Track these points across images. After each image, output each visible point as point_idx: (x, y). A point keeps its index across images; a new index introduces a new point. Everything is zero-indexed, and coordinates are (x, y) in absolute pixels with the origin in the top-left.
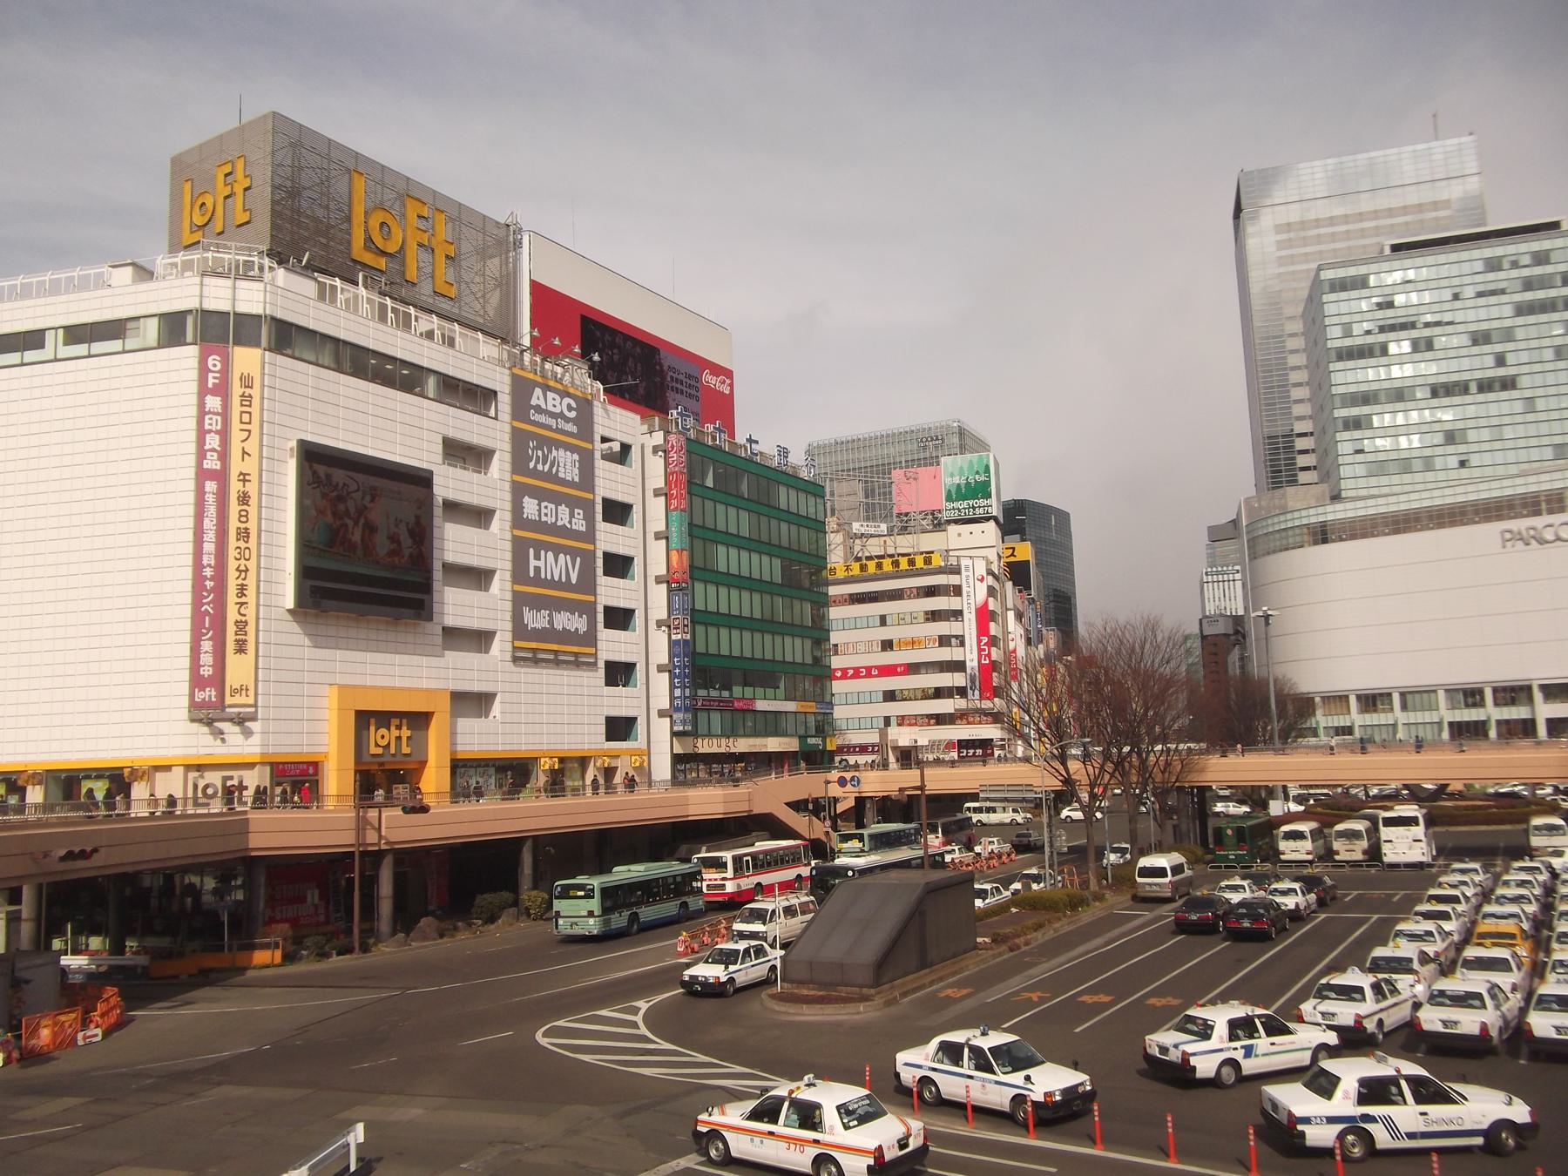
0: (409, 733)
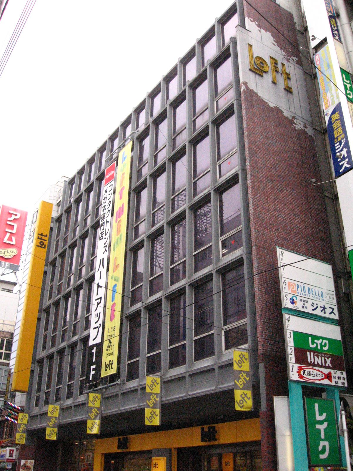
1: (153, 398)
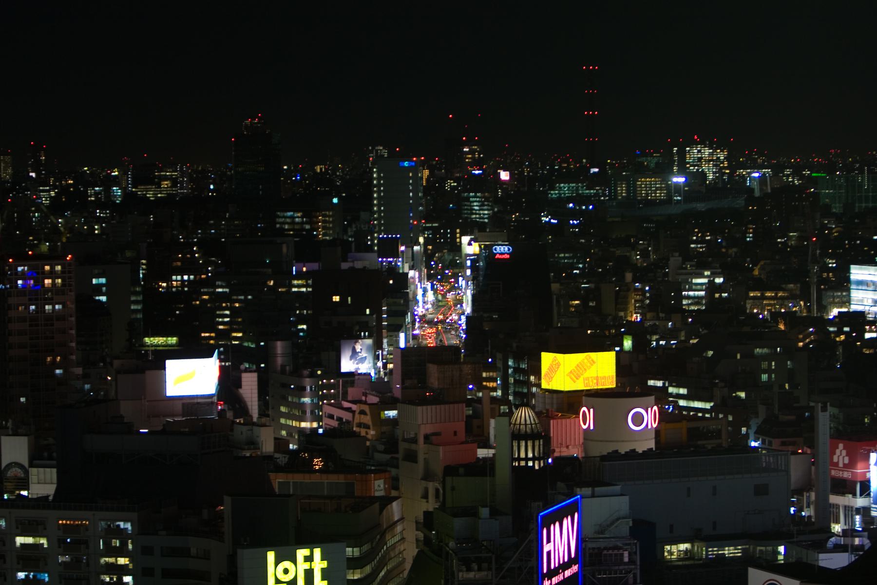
0: (325, 564)
1: (307, 566)
